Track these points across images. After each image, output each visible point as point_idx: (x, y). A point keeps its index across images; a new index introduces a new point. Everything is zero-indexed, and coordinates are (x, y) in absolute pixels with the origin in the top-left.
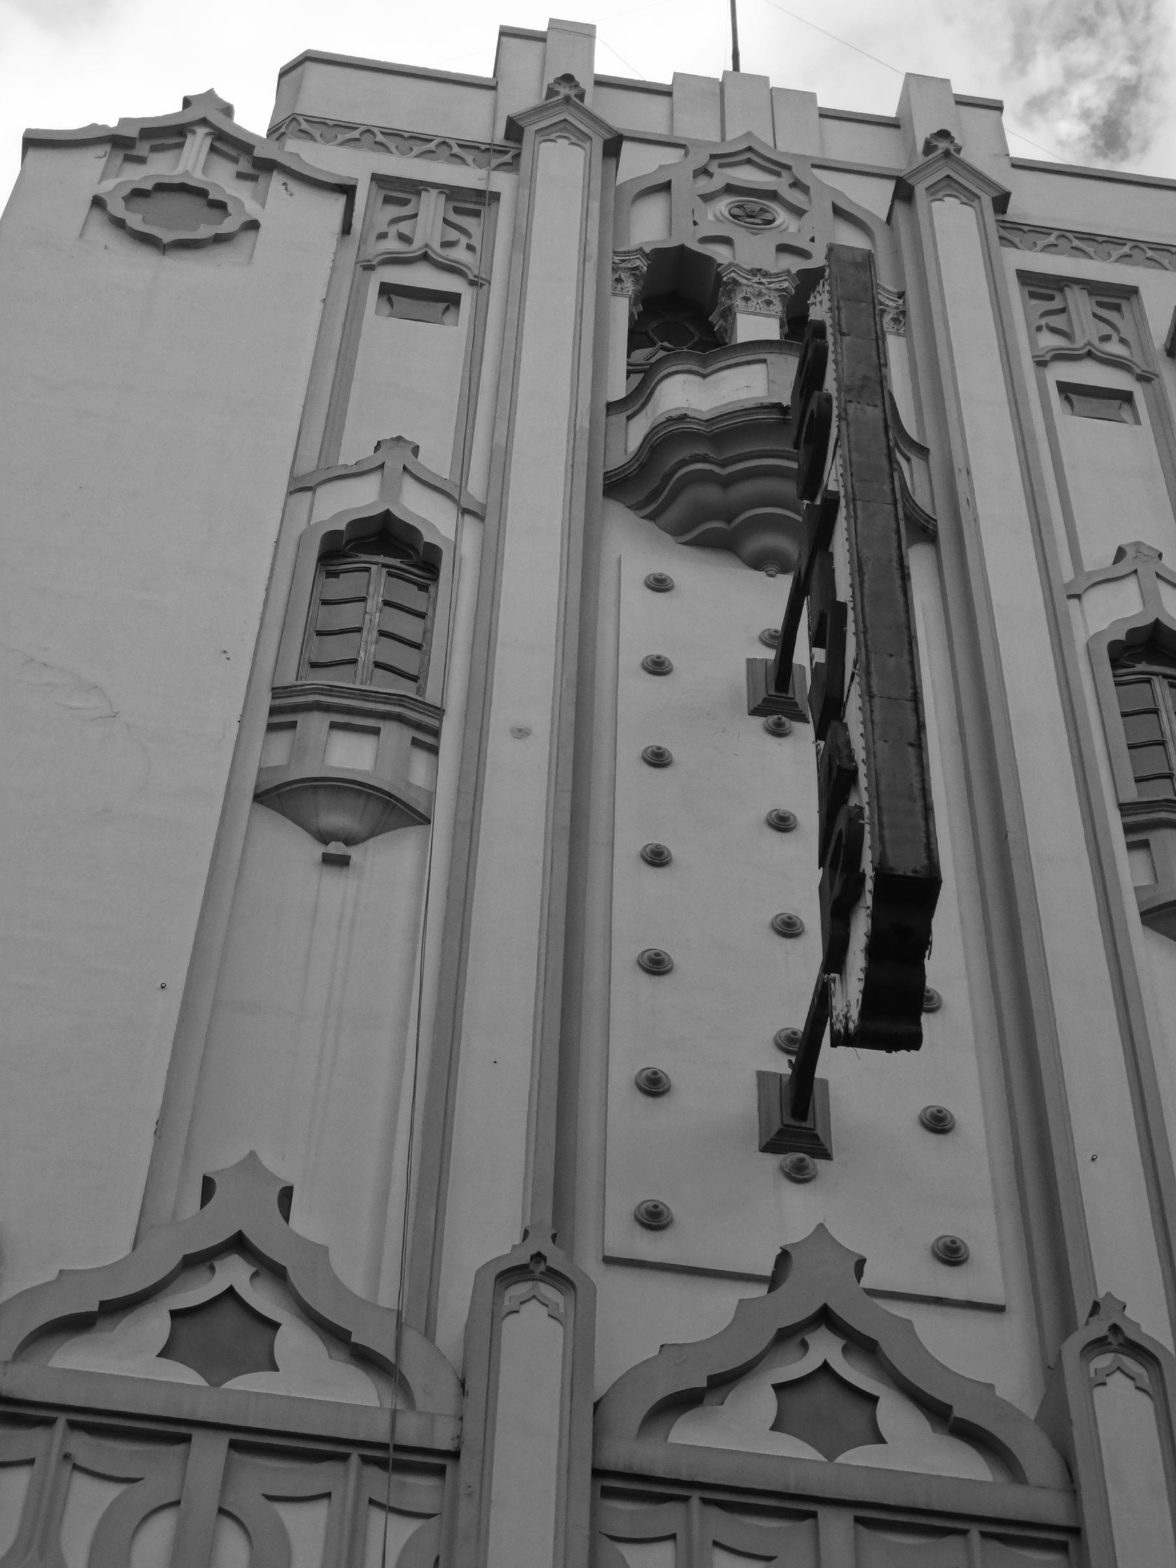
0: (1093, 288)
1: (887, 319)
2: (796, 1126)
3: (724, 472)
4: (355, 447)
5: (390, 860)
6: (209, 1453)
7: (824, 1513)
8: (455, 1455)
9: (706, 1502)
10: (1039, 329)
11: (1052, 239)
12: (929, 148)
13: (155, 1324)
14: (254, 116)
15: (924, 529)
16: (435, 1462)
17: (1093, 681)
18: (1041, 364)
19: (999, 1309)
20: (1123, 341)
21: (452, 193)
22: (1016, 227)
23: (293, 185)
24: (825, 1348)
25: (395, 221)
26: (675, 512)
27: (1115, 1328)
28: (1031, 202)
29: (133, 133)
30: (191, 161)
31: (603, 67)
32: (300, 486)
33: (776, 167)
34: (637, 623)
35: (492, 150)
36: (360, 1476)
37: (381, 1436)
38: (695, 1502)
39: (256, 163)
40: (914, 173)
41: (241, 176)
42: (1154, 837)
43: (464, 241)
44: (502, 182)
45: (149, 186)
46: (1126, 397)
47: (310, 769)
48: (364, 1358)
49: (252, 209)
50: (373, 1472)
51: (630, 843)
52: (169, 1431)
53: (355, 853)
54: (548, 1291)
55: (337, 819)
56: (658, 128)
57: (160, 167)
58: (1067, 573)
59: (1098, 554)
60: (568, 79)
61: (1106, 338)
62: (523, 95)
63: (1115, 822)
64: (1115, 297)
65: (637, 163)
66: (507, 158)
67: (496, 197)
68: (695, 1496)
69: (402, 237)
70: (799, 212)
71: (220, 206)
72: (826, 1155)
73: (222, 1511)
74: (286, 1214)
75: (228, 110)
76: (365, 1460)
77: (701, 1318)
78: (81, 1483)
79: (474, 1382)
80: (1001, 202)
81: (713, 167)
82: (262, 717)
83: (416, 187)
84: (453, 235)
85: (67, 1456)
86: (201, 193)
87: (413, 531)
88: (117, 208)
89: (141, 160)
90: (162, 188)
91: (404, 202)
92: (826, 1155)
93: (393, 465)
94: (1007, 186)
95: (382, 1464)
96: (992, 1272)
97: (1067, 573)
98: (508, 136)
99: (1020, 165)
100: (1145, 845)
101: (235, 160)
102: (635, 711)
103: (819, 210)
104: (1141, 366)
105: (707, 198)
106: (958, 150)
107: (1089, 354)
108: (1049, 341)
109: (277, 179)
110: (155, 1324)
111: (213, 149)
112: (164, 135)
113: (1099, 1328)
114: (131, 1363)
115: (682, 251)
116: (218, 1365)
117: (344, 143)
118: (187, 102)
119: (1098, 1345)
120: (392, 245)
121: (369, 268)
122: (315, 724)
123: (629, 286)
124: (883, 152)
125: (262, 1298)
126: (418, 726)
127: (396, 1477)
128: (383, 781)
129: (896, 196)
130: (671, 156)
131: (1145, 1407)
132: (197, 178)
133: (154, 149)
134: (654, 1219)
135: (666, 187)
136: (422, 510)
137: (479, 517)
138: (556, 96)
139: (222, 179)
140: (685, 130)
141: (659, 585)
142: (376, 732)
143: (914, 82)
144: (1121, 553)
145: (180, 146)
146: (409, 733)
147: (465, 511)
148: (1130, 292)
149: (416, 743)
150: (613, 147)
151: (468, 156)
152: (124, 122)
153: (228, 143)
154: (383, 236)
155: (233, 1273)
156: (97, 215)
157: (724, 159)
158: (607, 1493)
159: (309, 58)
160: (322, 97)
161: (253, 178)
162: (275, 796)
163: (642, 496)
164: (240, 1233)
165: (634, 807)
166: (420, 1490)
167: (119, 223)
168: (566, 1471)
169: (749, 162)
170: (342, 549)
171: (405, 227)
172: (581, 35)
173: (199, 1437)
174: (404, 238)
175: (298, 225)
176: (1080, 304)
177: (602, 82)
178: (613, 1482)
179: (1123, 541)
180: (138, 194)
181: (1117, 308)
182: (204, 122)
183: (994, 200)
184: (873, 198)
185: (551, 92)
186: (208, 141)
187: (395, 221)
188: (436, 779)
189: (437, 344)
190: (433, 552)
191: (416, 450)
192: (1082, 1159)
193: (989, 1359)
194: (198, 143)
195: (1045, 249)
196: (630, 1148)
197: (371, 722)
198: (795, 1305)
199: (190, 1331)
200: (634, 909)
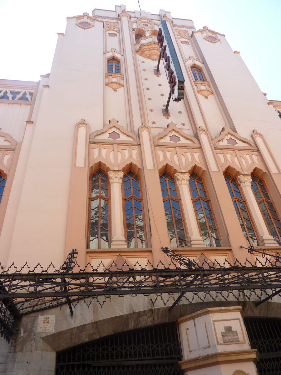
2: (166, 111)
3: (149, 50)
4: (109, 49)
5: (121, 91)
7: (176, 147)
14: (91, 15)
18: (179, 39)
24: (174, 133)
30: (85, 20)
32: (104, 54)
34: (141, 66)
46: (116, 34)
47: (110, 81)
49: (93, 24)
56: (134, 16)
57: (82, 20)
61: (115, 29)
62: (119, 12)
70: (151, 24)
72: (170, 116)
82: (105, 77)
92: (170, 116)
96: (188, 125)
102: (143, 75)
112: (83, 17)
118: (84, 13)
122: (110, 77)
125: (118, 131)
134: (154, 123)
138: (122, 13)
139: (89, 21)
141: (143, 62)
143: (161, 10)
146: (120, 78)
152: (77, 16)
153: (89, 17)
154: (107, 28)
155: (114, 129)
159: (95, 9)
162: (107, 84)
164: (114, 118)
165: (145, 84)
167: (79, 26)
172: (125, 6)
175: (98, 26)
177: (127, 12)
179: (190, 56)
189: (116, 39)
194: (86, 17)
198: (170, 129)
200: (147, 94)
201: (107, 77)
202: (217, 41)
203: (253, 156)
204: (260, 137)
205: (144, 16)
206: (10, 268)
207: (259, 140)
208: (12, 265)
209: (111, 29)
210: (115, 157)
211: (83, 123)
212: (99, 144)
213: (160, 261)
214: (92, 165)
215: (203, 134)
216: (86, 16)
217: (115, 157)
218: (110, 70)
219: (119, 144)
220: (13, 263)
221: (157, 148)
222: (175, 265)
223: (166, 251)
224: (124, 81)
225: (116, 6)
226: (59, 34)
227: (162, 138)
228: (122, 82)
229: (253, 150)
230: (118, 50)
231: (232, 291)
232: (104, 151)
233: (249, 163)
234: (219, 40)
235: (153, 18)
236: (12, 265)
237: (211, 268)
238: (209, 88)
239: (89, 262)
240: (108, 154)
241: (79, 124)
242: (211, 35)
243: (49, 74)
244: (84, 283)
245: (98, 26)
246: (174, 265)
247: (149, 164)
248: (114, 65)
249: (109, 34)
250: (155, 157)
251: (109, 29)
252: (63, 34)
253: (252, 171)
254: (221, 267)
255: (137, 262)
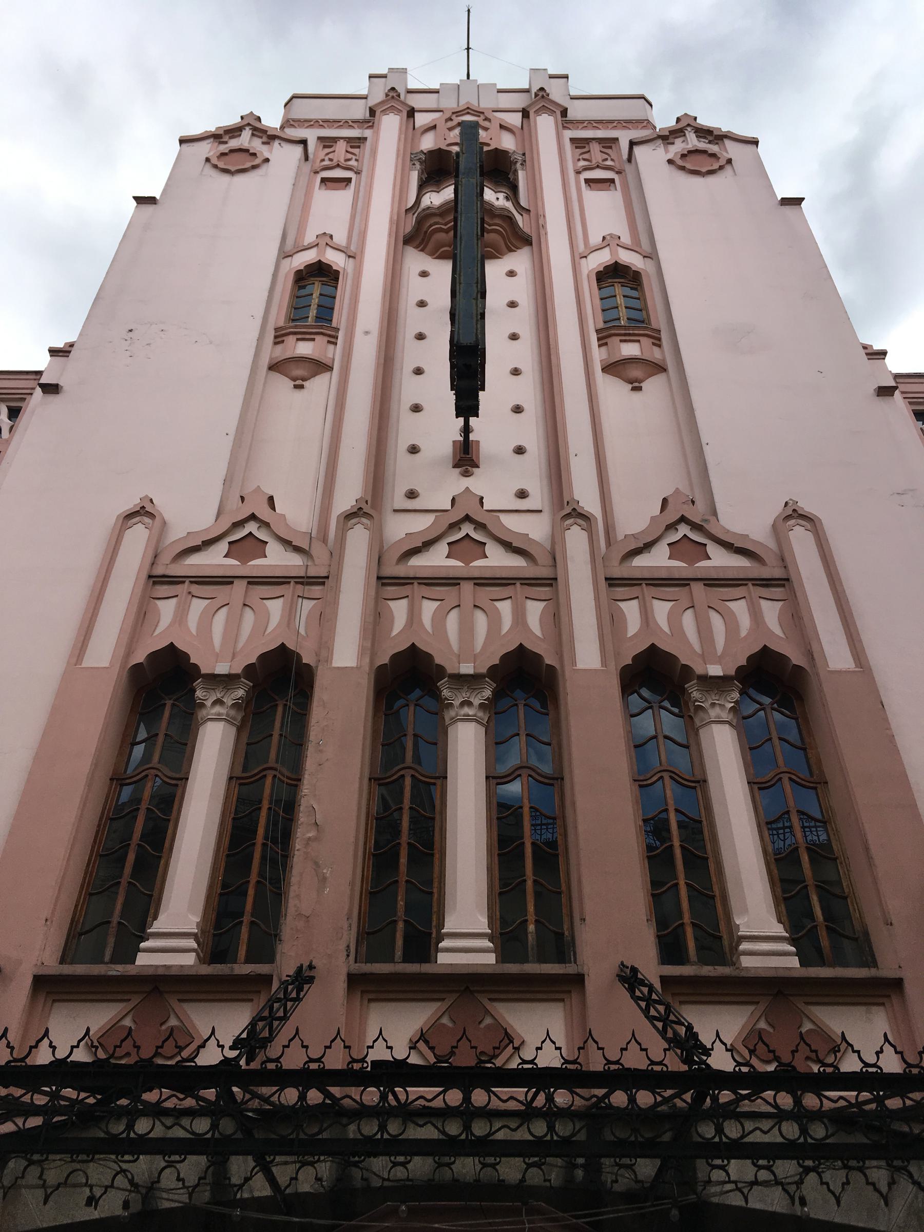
0: (600, 140)
1: (518, 165)
4: (310, 238)
5: (319, 386)
6: (240, 585)
8: (327, 577)
9: (419, 583)
10: (579, 160)
11: (585, 124)
12: (536, 95)
13: (223, 546)
14: (272, 120)
15: (527, 240)
16: (320, 581)
17: (589, 289)
18: (578, 172)
19: (541, 511)
20: (612, 160)
21: (349, 140)
22: (571, 122)
23: (283, 144)
24: (684, 530)
25: (327, 154)
26: (430, 246)
27: (574, 509)
28: (577, 111)
29: (221, 132)
30: (245, 140)
31: (412, 85)
32: (285, 254)
33: (478, 113)
34: (414, 288)
35: (365, 121)
36: (294, 588)
37: (302, 574)
38: (416, 584)
39: (270, 137)
40: (530, 106)
41: (264, 143)
42: (609, 340)
43: (354, 157)
44: (368, 133)
45: (227, 151)
46: (612, 181)
47: (288, 354)
48: (298, 549)
49: (267, 155)
50: (300, 586)
51: (408, 367)
52: (226, 581)
53: (306, 384)
54: (364, 520)
55: (299, 372)
57: (234, 143)
58: (581, 248)
59: (595, 239)
60: (393, 89)
61: (606, 159)
62: (378, 96)
63: (594, 337)
64: (609, 143)
65: (422, 120)
66: (370, 124)
67: (366, 139)
68: (416, 582)
69: (331, 160)
70: (486, 129)
71: (254, 155)
72: (478, 467)
73: (245, 605)
74: (274, 509)
75: (259, 119)
76: (296, 583)
77: (421, 524)
78: (195, 600)
79: (337, 555)
80: (564, 112)
81: (454, 117)
83: (335, 140)
84: (349, 156)
85: (190, 593)
86: (247, 151)
87: (330, 266)
88: (214, 161)
89: (226, 143)
90: (232, 151)
91: (331, 147)
93: (322, 242)
94: (566, 105)
95: (302, 583)
96: (538, 498)
97: (581, 248)
98: (370, 116)
99: (573, 98)
100: (606, 344)
101: (261, 137)
103: (494, 126)
104: (618, 167)
105: (450, 129)
106: (548, 95)
107: (598, 167)
108: (582, 163)
109: (277, 142)
110: (223, 546)
111: (253, 135)
112: (234, 131)
113: (568, 510)
114: (215, 559)
115: (440, 150)
116: (244, 559)
117: (307, 127)
118: (242, 118)
119: (568, 516)
120: (327, 163)
121: (316, 172)
122: (291, 339)
123: (418, 166)
124: (519, 101)
125: (262, 535)
126: (329, 336)
127: (307, 587)
128: (316, 356)
129: (523, 117)
130: (437, 115)
131: (584, 535)
132: (246, 145)
133: (231, 138)
135: (434, 127)
136: (335, 259)
137: (353, 257)
140: (442, 106)
141: (424, 274)
142: (313, 340)
144: (604, 238)
145: (240, 135)
146: (326, 339)
147: (349, 257)
148: (616, 140)
149: (329, 342)
150: (411, 113)
151: (355, 125)
152: (218, 128)
153: (259, 131)
154: (323, 160)
156: (208, 165)
157: (457, 113)
158: (384, 584)
159: (294, 97)
160: (303, 110)
161: (268, 143)
162: (274, 367)
163: (417, 242)
166: (316, 590)
167: (215, 166)
168: (368, 578)
169: (468, 113)
170: (303, 277)
171: (330, 156)
173: (236, 581)
174: (331, 160)
175: (285, 158)
176: (595, 148)
177: (410, 92)
178: (383, 580)
180: (223, 154)
181: (611, 147)
182: (249, 124)
183: (561, 112)
184: (515, 120)
185: (387, 95)
186: (250, 132)
187: (327, 154)
188: (334, 354)
189: (342, 198)
190: (337, 273)
191: (331, 237)
192: (572, 456)
193: (534, 529)
194: (247, 133)
195: (582, 129)
196: (404, 473)
197: (312, 337)
199: (234, 550)
201: (279, 337)
202: (721, 168)
203: (764, 603)
204: (809, 527)
205: (468, 103)
206: (288, 1046)
207: (800, 539)
208: (294, 1037)
209: (334, 163)
210: (467, 629)
211: (143, 512)
212: (746, 585)
213: (718, 1035)
214: (384, 659)
215: (575, 528)
216: (689, 129)
217: (467, 629)
218: (297, 311)
219: (712, 582)
220: (297, 1029)
221: (620, 591)
222: (646, 1050)
223: (630, 978)
224: (663, 353)
225: (371, 77)
226: (139, 200)
227: (637, 552)
228: (656, 354)
229: (766, 583)
230: (626, 239)
231: (909, 1162)
232: (429, 608)
233: (500, 629)
234: (729, 161)
235: (502, 106)
236: (294, 1037)
237: (870, 1070)
238: (656, 349)
239: (381, 1033)
240: (439, 619)
241: (130, 516)
242: (702, 145)
243: (72, 345)
244: (626, 1108)
245: (285, 158)
246: (642, 1049)
247: (587, 655)
248: (313, 292)
249: (588, 181)
250: (609, 624)
251: (586, 163)
252: (151, 200)
253: (498, 662)
254: (867, 1065)
255: (633, 1035)
